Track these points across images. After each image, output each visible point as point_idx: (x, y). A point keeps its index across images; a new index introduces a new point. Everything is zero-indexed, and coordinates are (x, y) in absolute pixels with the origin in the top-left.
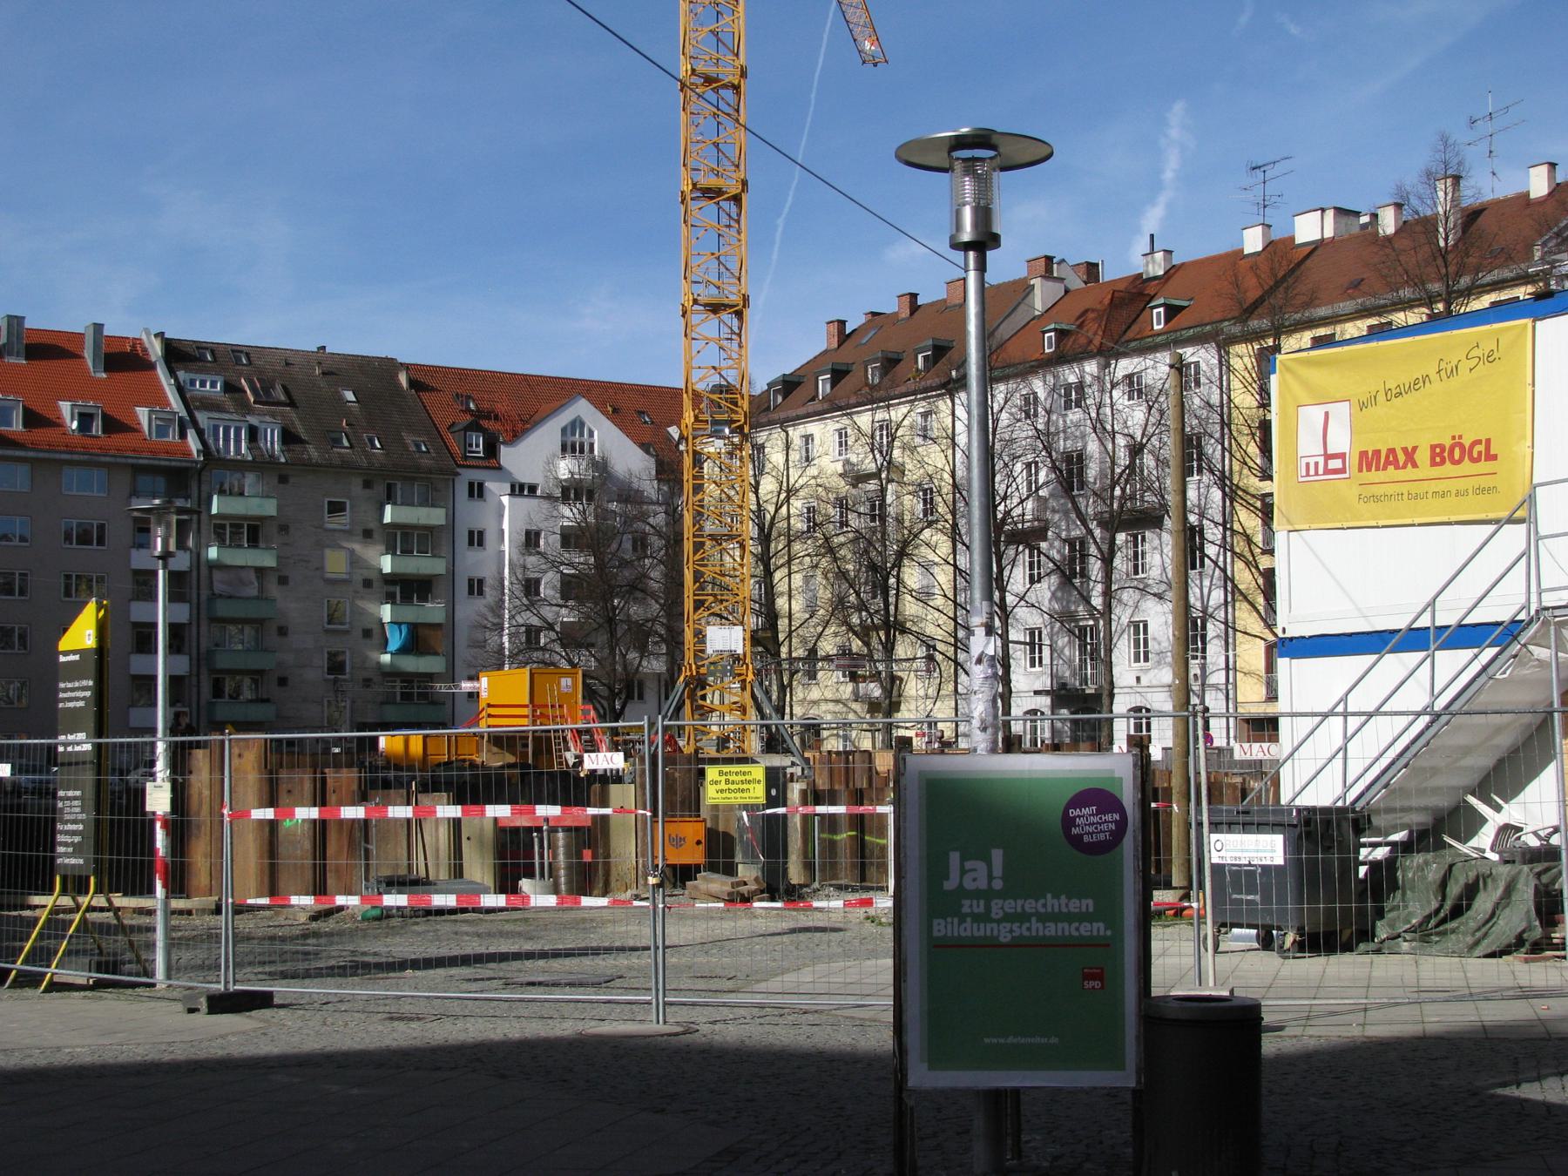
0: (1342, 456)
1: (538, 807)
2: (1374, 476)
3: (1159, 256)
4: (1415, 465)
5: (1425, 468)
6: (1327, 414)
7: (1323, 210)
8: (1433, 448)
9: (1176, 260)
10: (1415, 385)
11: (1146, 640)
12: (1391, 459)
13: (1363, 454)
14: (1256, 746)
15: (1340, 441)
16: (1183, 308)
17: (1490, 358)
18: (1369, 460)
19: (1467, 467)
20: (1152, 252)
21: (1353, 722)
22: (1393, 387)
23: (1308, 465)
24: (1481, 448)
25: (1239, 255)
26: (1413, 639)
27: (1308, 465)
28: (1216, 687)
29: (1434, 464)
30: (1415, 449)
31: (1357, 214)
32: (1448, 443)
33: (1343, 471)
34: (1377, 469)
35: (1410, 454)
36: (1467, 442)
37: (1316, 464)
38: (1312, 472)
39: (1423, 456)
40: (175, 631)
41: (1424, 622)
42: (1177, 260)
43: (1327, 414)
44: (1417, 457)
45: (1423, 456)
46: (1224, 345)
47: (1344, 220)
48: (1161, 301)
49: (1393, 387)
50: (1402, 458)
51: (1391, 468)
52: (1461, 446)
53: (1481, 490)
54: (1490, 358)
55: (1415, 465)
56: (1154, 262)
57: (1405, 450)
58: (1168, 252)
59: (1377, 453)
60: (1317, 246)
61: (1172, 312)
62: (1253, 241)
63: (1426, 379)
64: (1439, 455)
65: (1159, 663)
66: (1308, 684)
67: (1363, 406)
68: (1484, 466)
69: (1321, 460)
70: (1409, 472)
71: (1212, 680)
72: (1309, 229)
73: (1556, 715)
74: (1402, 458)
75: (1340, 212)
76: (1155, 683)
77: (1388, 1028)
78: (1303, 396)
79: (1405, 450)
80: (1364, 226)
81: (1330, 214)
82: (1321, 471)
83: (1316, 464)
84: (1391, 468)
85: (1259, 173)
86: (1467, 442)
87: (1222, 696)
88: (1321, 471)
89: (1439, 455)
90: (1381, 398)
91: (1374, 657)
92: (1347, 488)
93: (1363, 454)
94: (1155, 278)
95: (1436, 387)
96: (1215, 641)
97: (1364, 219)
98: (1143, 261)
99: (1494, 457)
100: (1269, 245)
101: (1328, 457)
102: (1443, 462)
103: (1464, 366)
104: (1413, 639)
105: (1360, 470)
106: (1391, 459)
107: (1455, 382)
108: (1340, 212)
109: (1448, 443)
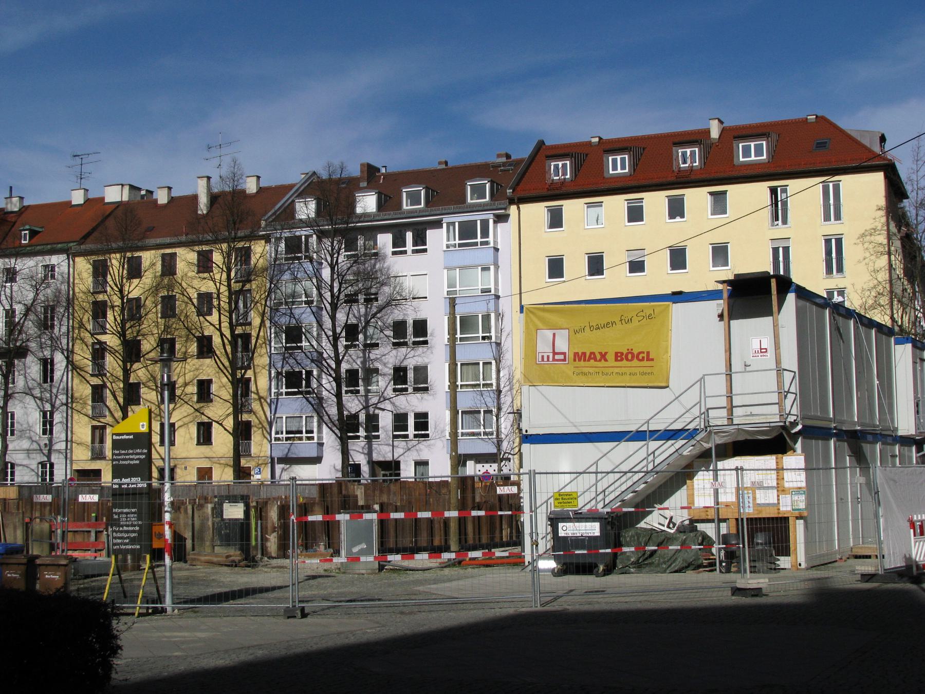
0: (564, 354)
1: (469, 553)
2: (582, 363)
3: (15, 200)
4: (606, 360)
5: (611, 361)
6: (554, 335)
7: (123, 185)
8: (616, 354)
9: (26, 203)
10: (607, 325)
11: (13, 425)
12: (592, 356)
13: (576, 354)
14: (506, 488)
15: (562, 345)
16: (40, 232)
17: (650, 317)
18: (579, 357)
19: (635, 362)
20: (11, 197)
21: (593, 469)
22: (594, 325)
23: (543, 357)
24: (645, 355)
25: (68, 204)
26: (639, 436)
27: (543, 357)
28: (59, 451)
29: (616, 360)
30: (606, 353)
31: (140, 189)
32: (625, 352)
33: (564, 360)
34: (585, 360)
35: (604, 356)
36: (635, 352)
37: (548, 357)
38: (545, 359)
39: (611, 357)
40: (377, 480)
41: (644, 428)
42: (26, 203)
43: (554, 335)
44: (607, 357)
45: (611, 357)
46: (72, 255)
47: (134, 192)
48: (27, 227)
49: (594, 325)
50: (598, 357)
51: (592, 361)
52: (632, 354)
53: (644, 374)
54: (650, 317)
55: (606, 360)
56: (11, 203)
57: (600, 353)
58: (21, 198)
59: (584, 354)
60: (119, 204)
61: (33, 234)
62: (78, 198)
63: (613, 323)
64: (619, 356)
65: (21, 437)
66: (534, 455)
67: (576, 332)
68: (645, 363)
69: (551, 355)
70: (603, 363)
71: (56, 447)
72: (113, 195)
73: (833, 466)
74: (598, 357)
75: (132, 187)
76: (17, 448)
77: (154, 624)
78: (540, 325)
79: (600, 353)
80: (143, 196)
81: (127, 189)
82: (551, 359)
83: (548, 357)
84: (592, 361)
85: (78, 160)
86: (635, 352)
87: (62, 456)
88: (551, 359)
89: (619, 356)
90: (587, 329)
91: (231, 431)
92: (568, 368)
93: (576, 354)
94: (12, 212)
95: (619, 325)
96: (59, 425)
97: (143, 193)
98: (4, 201)
99: (652, 360)
100: (88, 201)
101: (554, 353)
102: (622, 360)
103: (635, 319)
104: (639, 436)
105: (575, 360)
106: (592, 356)
107: (630, 326)
108: (132, 187)
109: (625, 352)
